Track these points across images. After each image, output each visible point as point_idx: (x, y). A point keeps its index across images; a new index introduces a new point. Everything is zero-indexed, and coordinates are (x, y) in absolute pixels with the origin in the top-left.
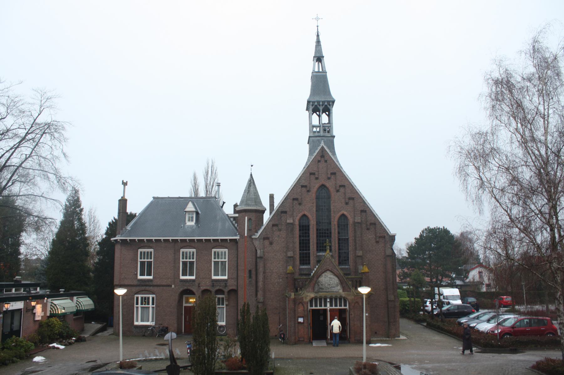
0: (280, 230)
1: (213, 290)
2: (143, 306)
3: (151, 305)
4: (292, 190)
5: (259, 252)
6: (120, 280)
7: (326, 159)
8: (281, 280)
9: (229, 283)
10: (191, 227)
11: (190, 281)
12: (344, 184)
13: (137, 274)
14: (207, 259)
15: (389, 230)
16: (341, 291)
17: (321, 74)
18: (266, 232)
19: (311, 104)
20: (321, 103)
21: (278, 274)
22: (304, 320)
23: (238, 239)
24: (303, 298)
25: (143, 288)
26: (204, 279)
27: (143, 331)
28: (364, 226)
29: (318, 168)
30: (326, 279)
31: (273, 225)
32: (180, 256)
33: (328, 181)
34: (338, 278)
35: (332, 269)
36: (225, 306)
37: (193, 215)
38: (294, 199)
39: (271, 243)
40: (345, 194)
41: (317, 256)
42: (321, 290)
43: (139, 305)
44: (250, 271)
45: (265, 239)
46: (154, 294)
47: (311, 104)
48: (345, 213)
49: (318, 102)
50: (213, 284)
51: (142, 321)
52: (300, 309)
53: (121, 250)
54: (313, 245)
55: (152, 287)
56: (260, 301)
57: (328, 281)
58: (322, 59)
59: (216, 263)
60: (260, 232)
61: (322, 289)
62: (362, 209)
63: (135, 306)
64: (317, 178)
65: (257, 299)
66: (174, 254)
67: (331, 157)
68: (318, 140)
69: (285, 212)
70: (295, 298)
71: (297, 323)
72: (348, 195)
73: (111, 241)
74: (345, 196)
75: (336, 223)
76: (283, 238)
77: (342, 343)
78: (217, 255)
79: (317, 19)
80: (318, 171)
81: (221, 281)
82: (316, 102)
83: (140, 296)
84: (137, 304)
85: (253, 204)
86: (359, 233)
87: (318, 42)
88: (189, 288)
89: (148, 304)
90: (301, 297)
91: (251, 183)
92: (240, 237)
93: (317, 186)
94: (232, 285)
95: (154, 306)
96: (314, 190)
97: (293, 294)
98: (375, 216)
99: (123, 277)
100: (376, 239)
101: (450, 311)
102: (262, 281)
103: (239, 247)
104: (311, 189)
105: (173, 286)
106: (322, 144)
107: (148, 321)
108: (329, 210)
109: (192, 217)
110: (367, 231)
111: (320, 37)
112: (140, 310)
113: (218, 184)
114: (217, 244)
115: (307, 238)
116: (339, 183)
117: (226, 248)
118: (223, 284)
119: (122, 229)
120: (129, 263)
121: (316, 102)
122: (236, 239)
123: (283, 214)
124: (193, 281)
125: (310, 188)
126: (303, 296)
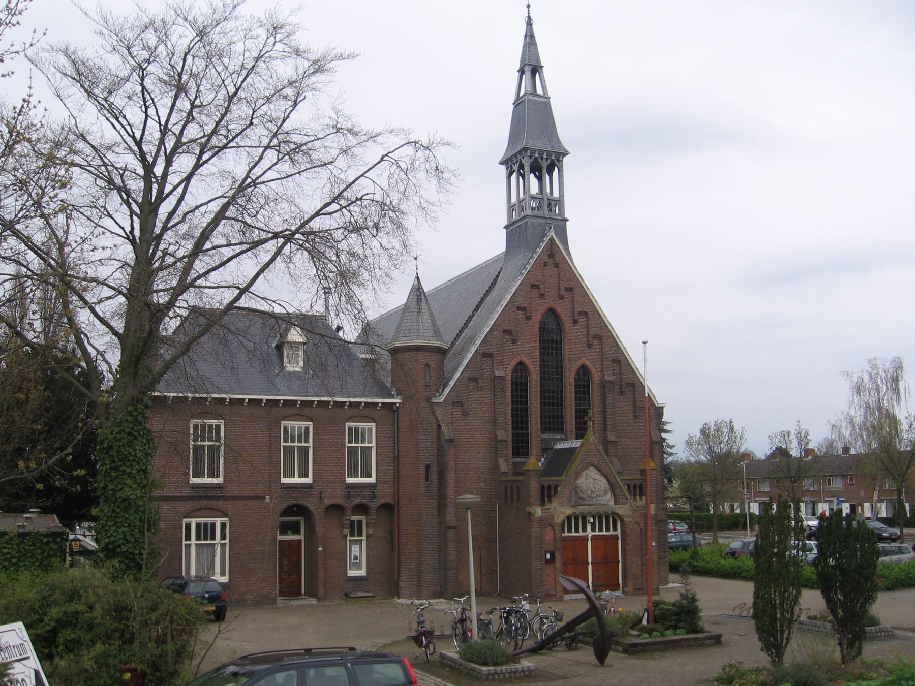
0: (479, 389)
1: (349, 505)
7: (557, 261)
8: (482, 485)
9: (379, 491)
16: (612, 503)
20: (545, 153)
21: (477, 472)
25: (204, 503)
26: (331, 483)
28: (617, 387)
30: (588, 482)
31: (470, 379)
34: (608, 480)
35: (598, 463)
36: (364, 537)
38: (505, 332)
39: (465, 413)
40: (587, 328)
41: (543, 440)
42: (581, 502)
43: (193, 541)
44: (428, 467)
48: (587, 363)
49: (541, 152)
50: (349, 493)
55: (221, 501)
59: (289, 451)
60: (447, 390)
63: (184, 542)
64: (542, 296)
65: (441, 522)
68: (541, 224)
71: (544, 562)
72: (592, 332)
74: (588, 332)
75: (572, 380)
78: (356, 435)
83: (194, 522)
84: (188, 538)
87: (530, 39)
89: (213, 538)
91: (420, 294)
93: (542, 310)
94: (386, 495)
95: (227, 541)
96: (537, 318)
100: (635, 412)
105: (268, 498)
106: (552, 233)
111: (534, 27)
114: (356, 411)
116: (579, 308)
118: (367, 493)
122: (395, 404)
124: (308, 486)
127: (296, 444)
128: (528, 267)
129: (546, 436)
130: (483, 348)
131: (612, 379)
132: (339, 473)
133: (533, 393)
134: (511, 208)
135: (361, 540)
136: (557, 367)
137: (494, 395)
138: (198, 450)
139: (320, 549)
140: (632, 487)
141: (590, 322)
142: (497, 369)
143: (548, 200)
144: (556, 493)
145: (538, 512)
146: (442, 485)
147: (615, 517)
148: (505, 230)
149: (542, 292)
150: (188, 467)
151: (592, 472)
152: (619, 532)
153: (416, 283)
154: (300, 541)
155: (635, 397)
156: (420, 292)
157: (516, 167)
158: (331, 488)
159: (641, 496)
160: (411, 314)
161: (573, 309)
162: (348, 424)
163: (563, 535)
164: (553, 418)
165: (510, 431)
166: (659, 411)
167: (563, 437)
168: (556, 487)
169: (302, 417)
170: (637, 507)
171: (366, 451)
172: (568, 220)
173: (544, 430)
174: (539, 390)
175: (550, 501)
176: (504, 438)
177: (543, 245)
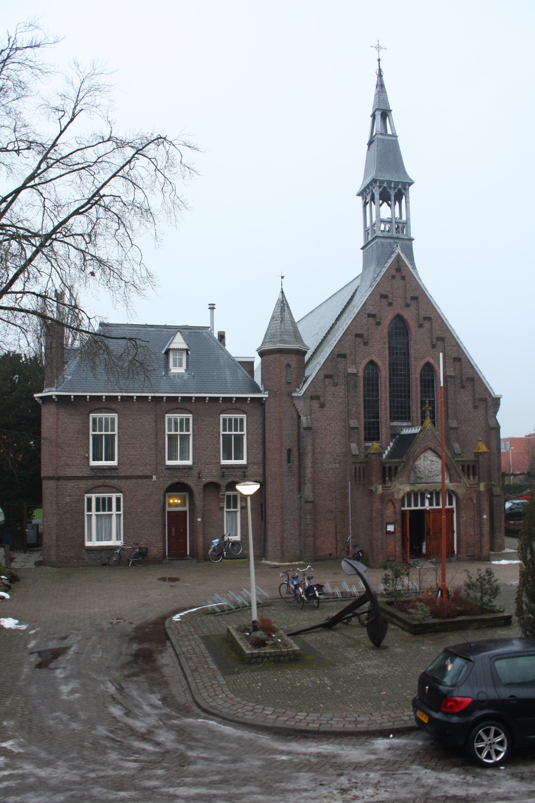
0: (336, 385)
2: (101, 513)
3: (114, 511)
5: (303, 419)
6: (57, 468)
7: (404, 275)
8: (337, 465)
10: (180, 376)
11: (185, 469)
12: (430, 316)
13: (88, 458)
14: (212, 431)
15: (492, 390)
17: (389, 138)
18: (314, 387)
19: (378, 184)
20: (393, 184)
21: (332, 455)
22: (395, 529)
23: (266, 398)
24: (393, 492)
25: (100, 482)
26: (207, 464)
27: (102, 556)
28: (458, 381)
29: (392, 287)
30: (426, 463)
31: (326, 376)
32: (164, 425)
33: (406, 309)
36: (239, 509)
37: (182, 356)
39: (322, 406)
41: (392, 428)
42: (419, 481)
43: (94, 512)
44: (289, 451)
45: (312, 398)
46: (121, 492)
47: (378, 184)
49: (389, 182)
50: (223, 472)
51: (98, 540)
52: (389, 511)
53: (58, 414)
54: (385, 409)
55: (116, 480)
56: (310, 500)
57: (429, 466)
58: (389, 114)
59: (227, 438)
61: (421, 478)
62: (456, 356)
63: (86, 513)
64: (390, 304)
66: (156, 421)
67: (411, 272)
68: (390, 244)
69: (344, 356)
70: (383, 493)
71: (384, 533)
73: (34, 398)
74: (432, 334)
75: (418, 376)
76: (341, 398)
79: (378, 48)
81: (237, 468)
82: (385, 183)
84: (90, 509)
85: (292, 340)
86: (452, 393)
88: (183, 480)
89: (110, 509)
90: (391, 491)
91: (284, 306)
92: (269, 394)
93: (390, 316)
95: (121, 512)
96: (386, 322)
97: (380, 487)
98: (472, 367)
99: (62, 463)
100: (474, 402)
101: (513, 511)
102: (311, 467)
103: (266, 411)
104: (381, 321)
105: (154, 478)
106: (398, 250)
107: (110, 539)
108: (407, 354)
109: (181, 360)
110: (461, 390)
112: (94, 519)
113: (212, 306)
114: (229, 405)
115: (374, 399)
116: (423, 314)
117: (245, 413)
119: (57, 378)
120: (72, 437)
121: (385, 183)
122: (262, 398)
123: (339, 359)
125: (380, 319)
126: (394, 490)
127: (104, 433)
128: (378, 279)
129: (395, 424)
130: (338, 349)
131: (453, 374)
132: (215, 456)
133: (383, 387)
134: (366, 232)
135: (236, 512)
136: (405, 364)
137: (348, 390)
138: (227, 438)
139: (199, 520)
140: (466, 468)
141: (434, 325)
142: (350, 367)
143: (396, 223)
144: (396, 472)
145: (380, 489)
146: (301, 466)
147: (451, 493)
148: (362, 251)
149: (390, 301)
150: (88, 452)
151: (430, 456)
152: (454, 506)
153: (281, 296)
154: (186, 512)
155: (474, 390)
156: (284, 304)
157: (369, 198)
158: (208, 468)
159: (474, 475)
160: (276, 322)
161: (418, 315)
162: (222, 416)
163: (403, 509)
164: (401, 407)
165: (362, 420)
166: (496, 402)
167: (410, 424)
168: (396, 468)
169: (183, 411)
170: (470, 485)
171: (110, 439)
172: (413, 239)
173: (393, 418)
174: (388, 385)
175: (391, 480)
176: (356, 425)
177: (390, 261)
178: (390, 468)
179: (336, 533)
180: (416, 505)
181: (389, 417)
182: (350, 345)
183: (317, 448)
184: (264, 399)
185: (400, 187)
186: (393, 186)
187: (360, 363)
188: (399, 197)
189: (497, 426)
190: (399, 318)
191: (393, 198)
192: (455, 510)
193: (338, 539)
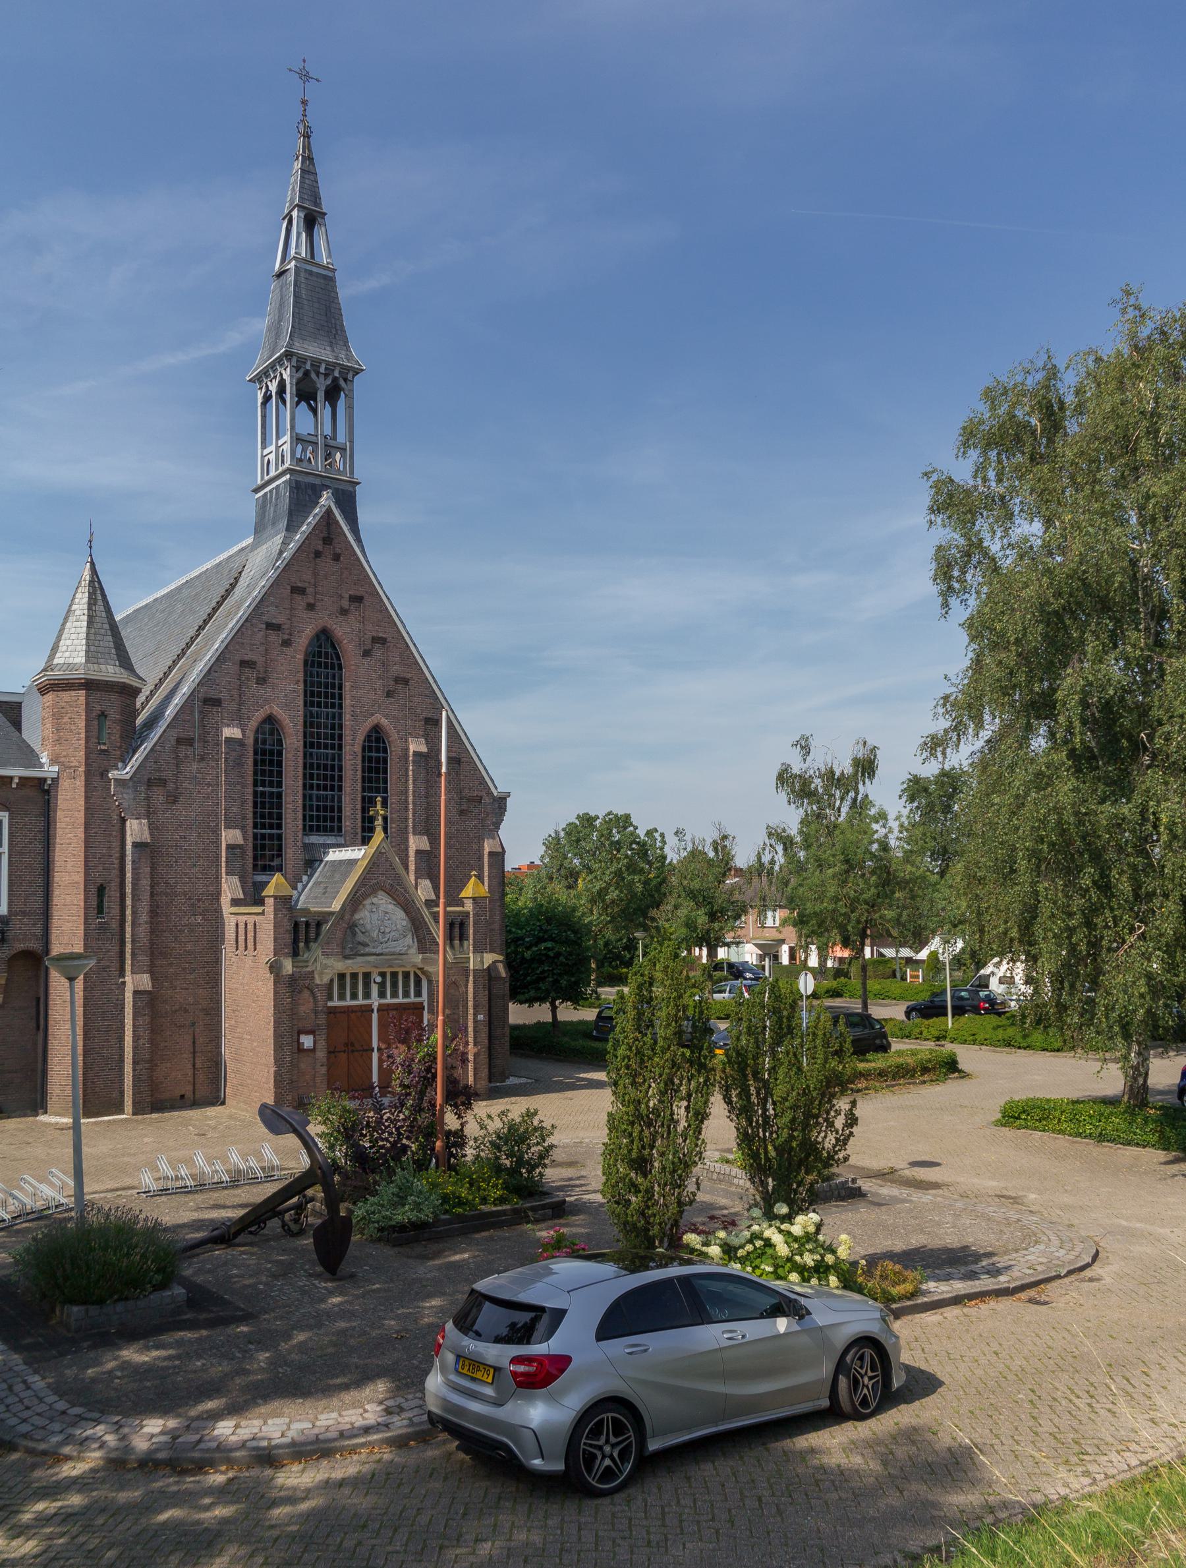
4: (240, 634)
7: (338, 550)
12: (384, 636)
20: (323, 367)
21: (190, 899)
41: (307, 847)
48: (384, 722)
49: (316, 363)
61: (366, 945)
64: (311, 607)
77: (1117, 1096)
79: (305, 76)
80: (315, 586)
115: (275, 790)
121: (309, 363)
129: (314, 839)
147: (419, 973)
156: (94, 587)
163: (330, 1004)
173: (309, 829)
175: (307, 947)
178: (307, 924)
179: (194, 1052)
180: (354, 996)
181: (301, 827)
182: (230, 682)
183: (158, 884)
184: (49, 782)
185: (336, 374)
186: (322, 370)
187: (249, 718)
188: (332, 394)
189: (500, 850)
190: (324, 637)
191: (321, 396)
192: (425, 1004)
193: (198, 1065)
